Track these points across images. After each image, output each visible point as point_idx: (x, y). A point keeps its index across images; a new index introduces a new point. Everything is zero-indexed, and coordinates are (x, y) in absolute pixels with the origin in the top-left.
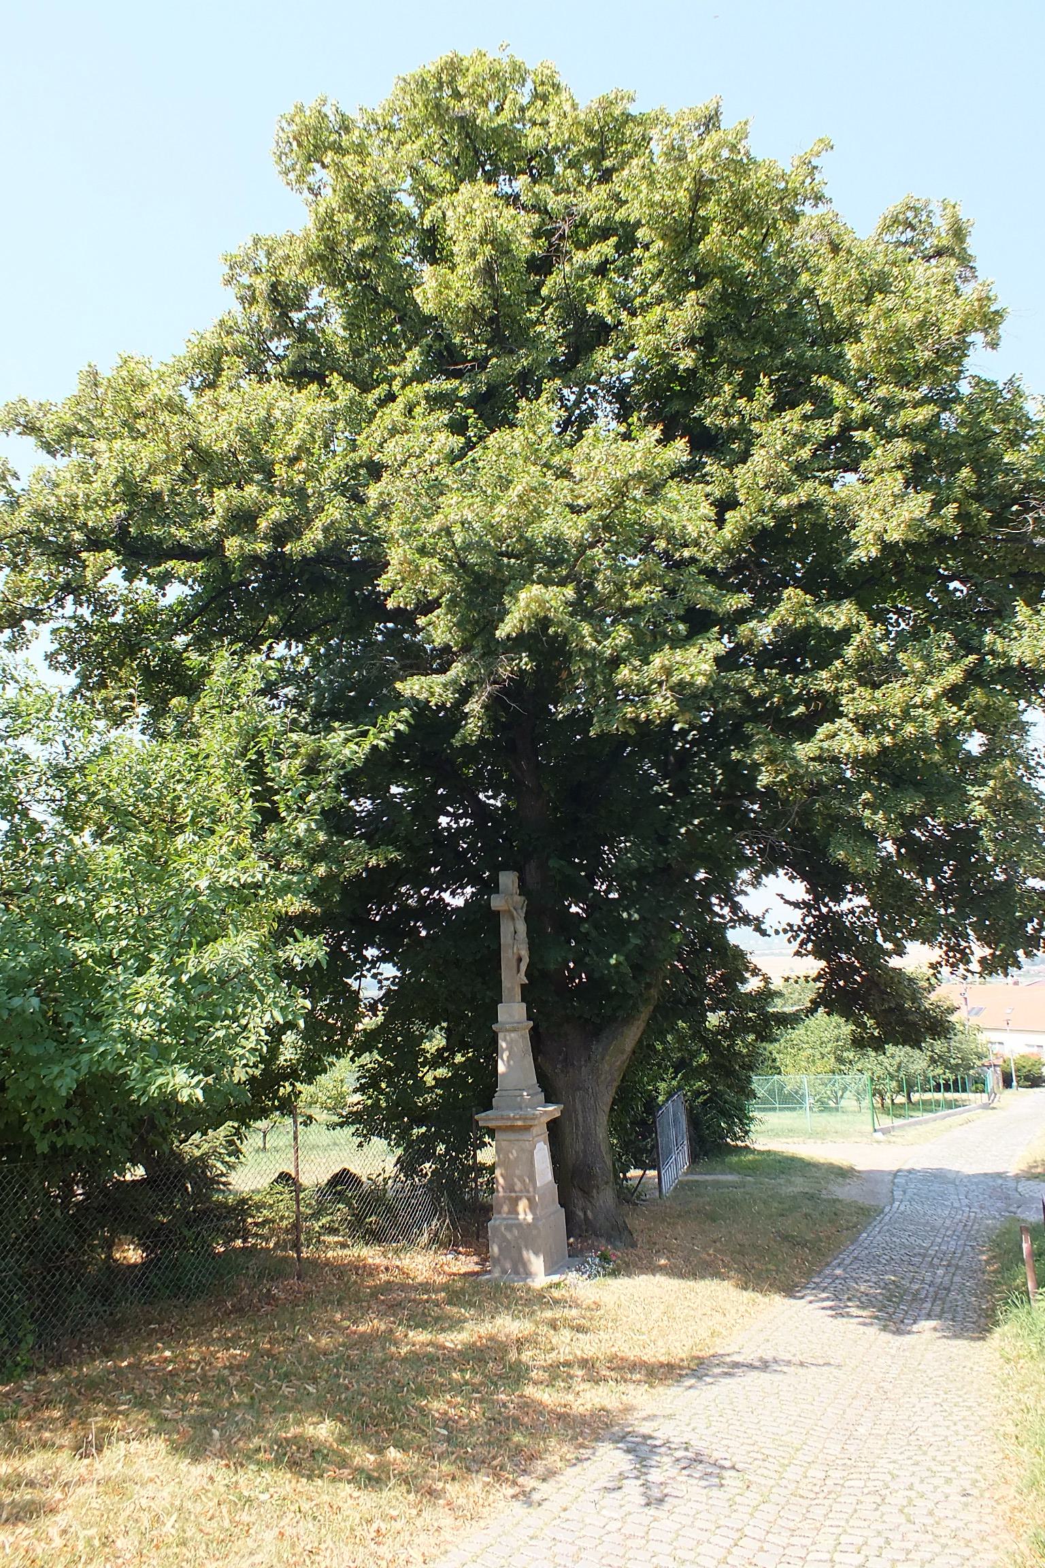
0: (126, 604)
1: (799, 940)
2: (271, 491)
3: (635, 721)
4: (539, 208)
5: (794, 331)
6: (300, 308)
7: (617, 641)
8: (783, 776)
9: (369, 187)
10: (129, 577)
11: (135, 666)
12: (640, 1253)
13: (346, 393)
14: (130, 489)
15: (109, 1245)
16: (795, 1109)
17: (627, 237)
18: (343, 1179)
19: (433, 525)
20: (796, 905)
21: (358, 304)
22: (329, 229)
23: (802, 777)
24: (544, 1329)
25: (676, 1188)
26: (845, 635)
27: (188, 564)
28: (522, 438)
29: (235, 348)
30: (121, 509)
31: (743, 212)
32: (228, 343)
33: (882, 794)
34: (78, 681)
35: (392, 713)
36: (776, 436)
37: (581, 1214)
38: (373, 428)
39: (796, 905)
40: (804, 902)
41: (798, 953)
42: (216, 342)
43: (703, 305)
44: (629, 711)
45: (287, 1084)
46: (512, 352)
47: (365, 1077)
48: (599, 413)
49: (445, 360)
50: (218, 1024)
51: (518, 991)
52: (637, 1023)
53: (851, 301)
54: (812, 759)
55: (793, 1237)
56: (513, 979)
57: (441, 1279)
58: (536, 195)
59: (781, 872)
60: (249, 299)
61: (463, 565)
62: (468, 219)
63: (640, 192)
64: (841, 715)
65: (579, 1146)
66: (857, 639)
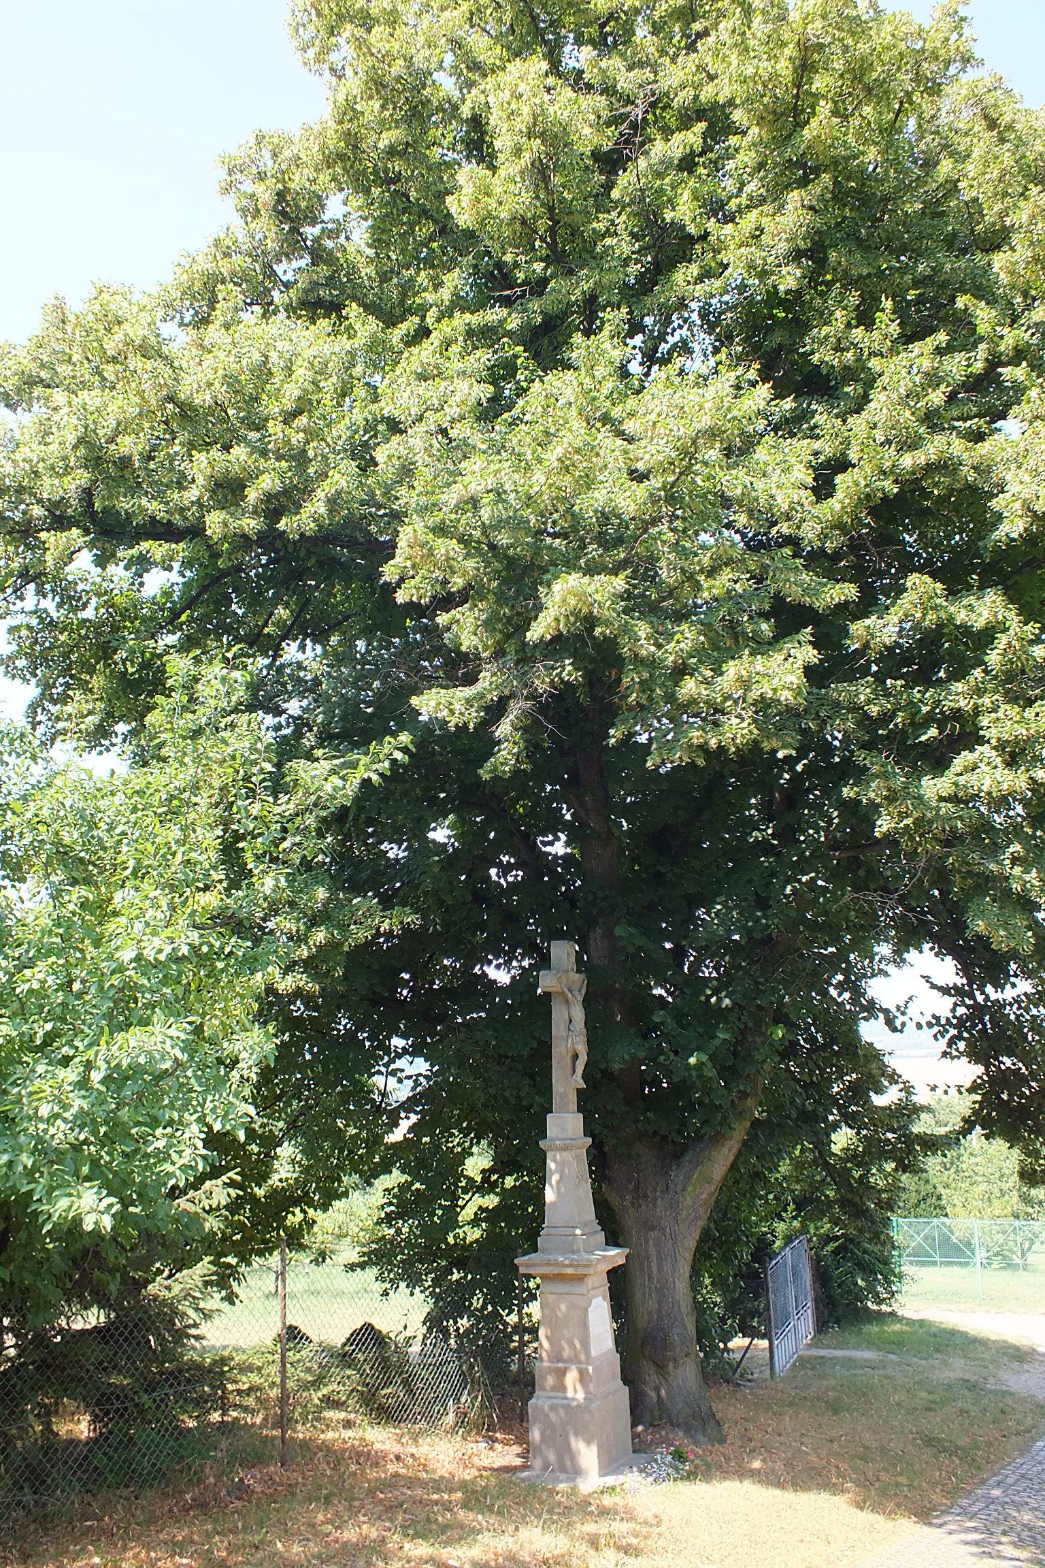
0: (98, 595)
1: (948, 1036)
2: (264, 453)
3: (703, 748)
4: (609, 90)
5: (930, 237)
6: (314, 222)
7: (682, 645)
8: (909, 821)
9: (398, 68)
10: (101, 562)
11: (102, 670)
12: (729, 1452)
13: (365, 327)
14: (94, 455)
15: (46, 1414)
16: (967, 1264)
17: (717, 122)
18: (368, 1336)
19: (451, 497)
20: (945, 990)
21: (387, 215)
22: (350, 121)
23: (930, 822)
24: (583, 1548)
25: (794, 1365)
26: (986, 637)
27: (166, 546)
28: (575, 383)
29: (233, 274)
30: (82, 477)
31: (862, 82)
32: (225, 268)
33: (1036, 846)
34: (39, 690)
35: (388, 738)
36: (905, 373)
37: (653, 1394)
38: (398, 372)
39: (945, 990)
40: (955, 987)
41: (945, 1054)
42: (210, 267)
43: (811, 208)
44: (696, 736)
45: (297, 1211)
46: (571, 272)
47: (391, 1204)
48: (696, 347)
49: (496, 283)
50: (159, 1131)
51: (573, 1097)
52: (728, 1144)
53: (1005, 194)
54: (942, 799)
55: (939, 1440)
56: (567, 1082)
57: (469, 1475)
58: (603, 71)
59: (926, 947)
60: (250, 212)
61: (493, 547)
62: (513, 106)
63: (730, 64)
64: (982, 741)
65: (652, 1304)
66: (1002, 640)
